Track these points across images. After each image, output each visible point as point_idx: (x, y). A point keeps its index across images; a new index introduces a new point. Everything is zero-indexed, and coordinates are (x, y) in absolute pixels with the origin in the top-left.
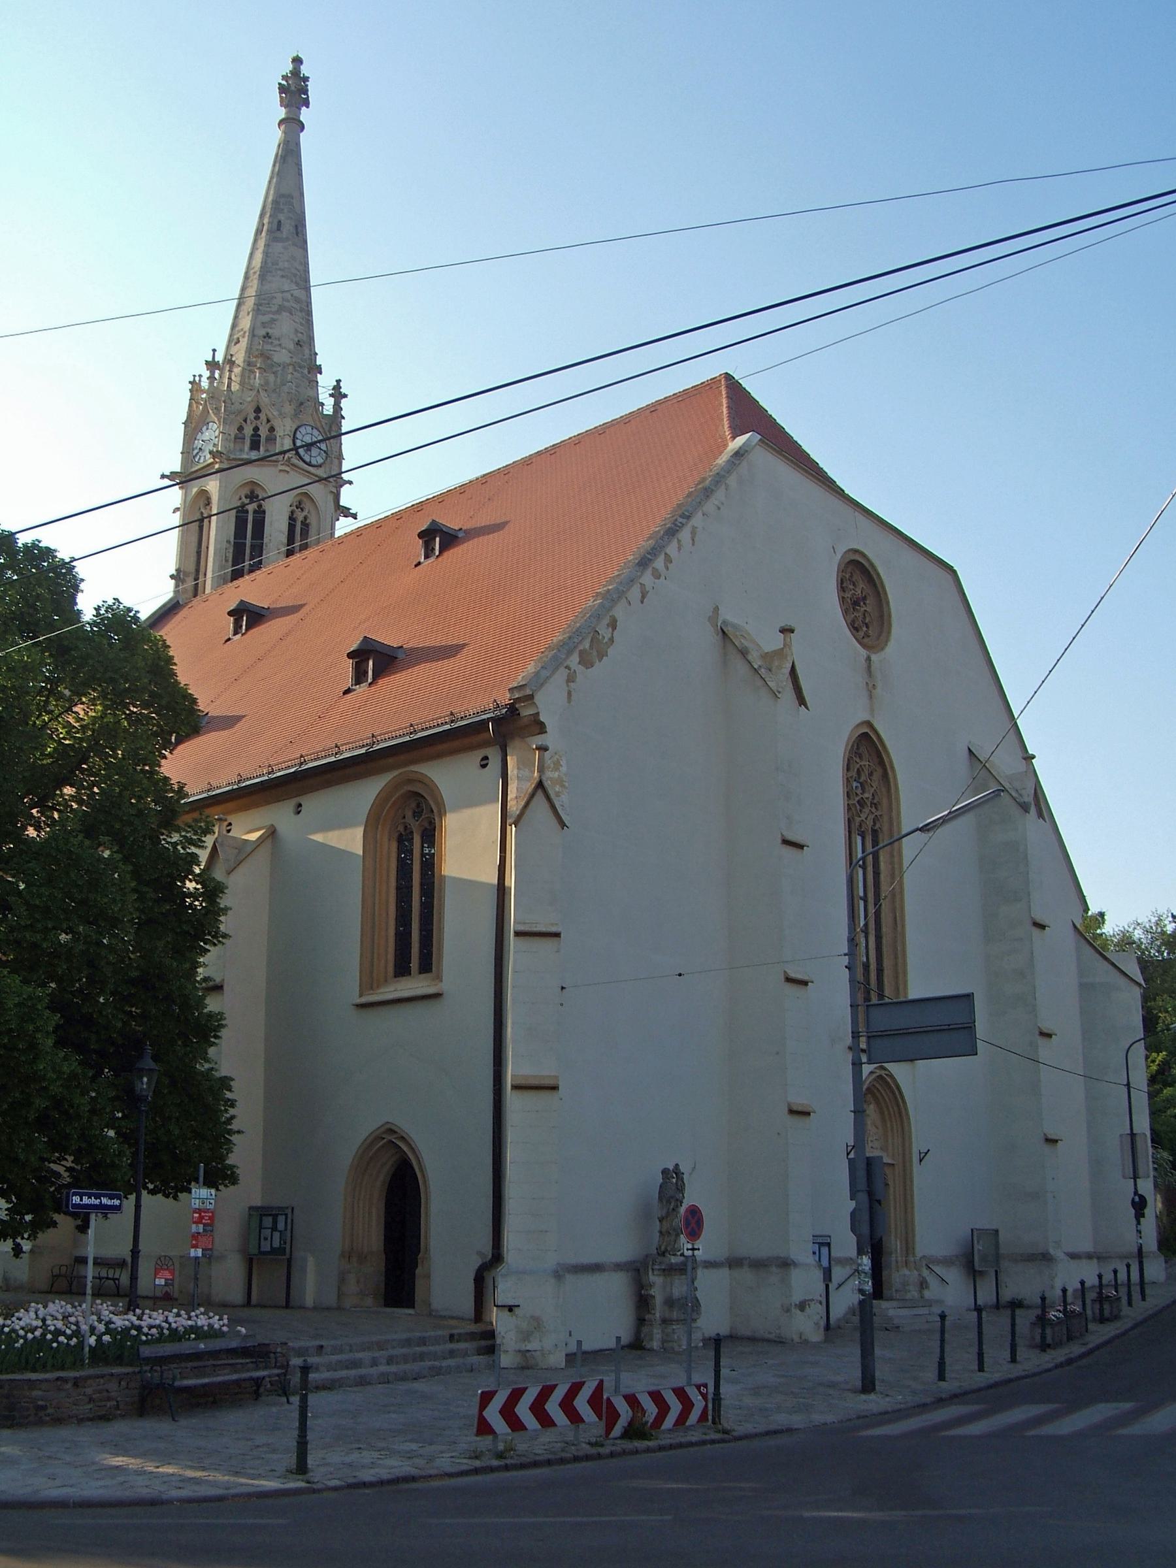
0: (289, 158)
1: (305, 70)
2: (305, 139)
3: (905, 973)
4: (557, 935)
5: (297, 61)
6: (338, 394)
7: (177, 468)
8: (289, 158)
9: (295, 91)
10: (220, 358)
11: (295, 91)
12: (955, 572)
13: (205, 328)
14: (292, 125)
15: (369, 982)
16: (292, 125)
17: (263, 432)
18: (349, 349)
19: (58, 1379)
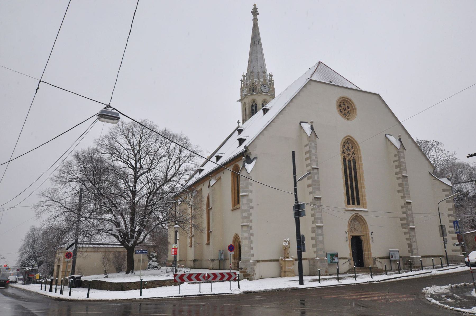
0: (255, 27)
1: (257, 7)
2: (259, 22)
3: (232, 198)
4: (468, 157)
5: (255, 5)
6: (271, 76)
7: (240, 99)
8: (255, 27)
9: (255, 12)
10: (245, 74)
11: (255, 12)
12: (378, 95)
13: (242, 67)
14: (255, 20)
15: (233, 207)
16: (255, 20)
17: (255, 88)
18: (271, 67)
19: (93, 247)
